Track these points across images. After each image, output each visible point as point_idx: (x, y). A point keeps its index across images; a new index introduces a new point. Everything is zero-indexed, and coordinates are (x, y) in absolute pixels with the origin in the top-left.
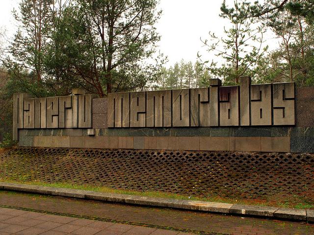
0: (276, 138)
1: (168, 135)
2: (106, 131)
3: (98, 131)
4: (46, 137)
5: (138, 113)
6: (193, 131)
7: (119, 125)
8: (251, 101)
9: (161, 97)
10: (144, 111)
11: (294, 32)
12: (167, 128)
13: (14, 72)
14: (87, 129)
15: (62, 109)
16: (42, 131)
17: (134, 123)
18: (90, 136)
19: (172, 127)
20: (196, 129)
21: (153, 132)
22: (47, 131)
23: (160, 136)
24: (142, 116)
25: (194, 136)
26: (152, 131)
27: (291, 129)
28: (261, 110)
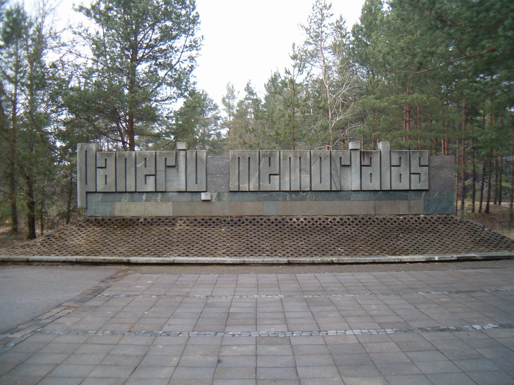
3: (215, 195)
12: (304, 192)
14: (200, 192)
16: (127, 195)
17: (266, 186)
21: (288, 197)
22: (136, 196)
23: (296, 200)
26: (287, 195)
28: (321, 183)
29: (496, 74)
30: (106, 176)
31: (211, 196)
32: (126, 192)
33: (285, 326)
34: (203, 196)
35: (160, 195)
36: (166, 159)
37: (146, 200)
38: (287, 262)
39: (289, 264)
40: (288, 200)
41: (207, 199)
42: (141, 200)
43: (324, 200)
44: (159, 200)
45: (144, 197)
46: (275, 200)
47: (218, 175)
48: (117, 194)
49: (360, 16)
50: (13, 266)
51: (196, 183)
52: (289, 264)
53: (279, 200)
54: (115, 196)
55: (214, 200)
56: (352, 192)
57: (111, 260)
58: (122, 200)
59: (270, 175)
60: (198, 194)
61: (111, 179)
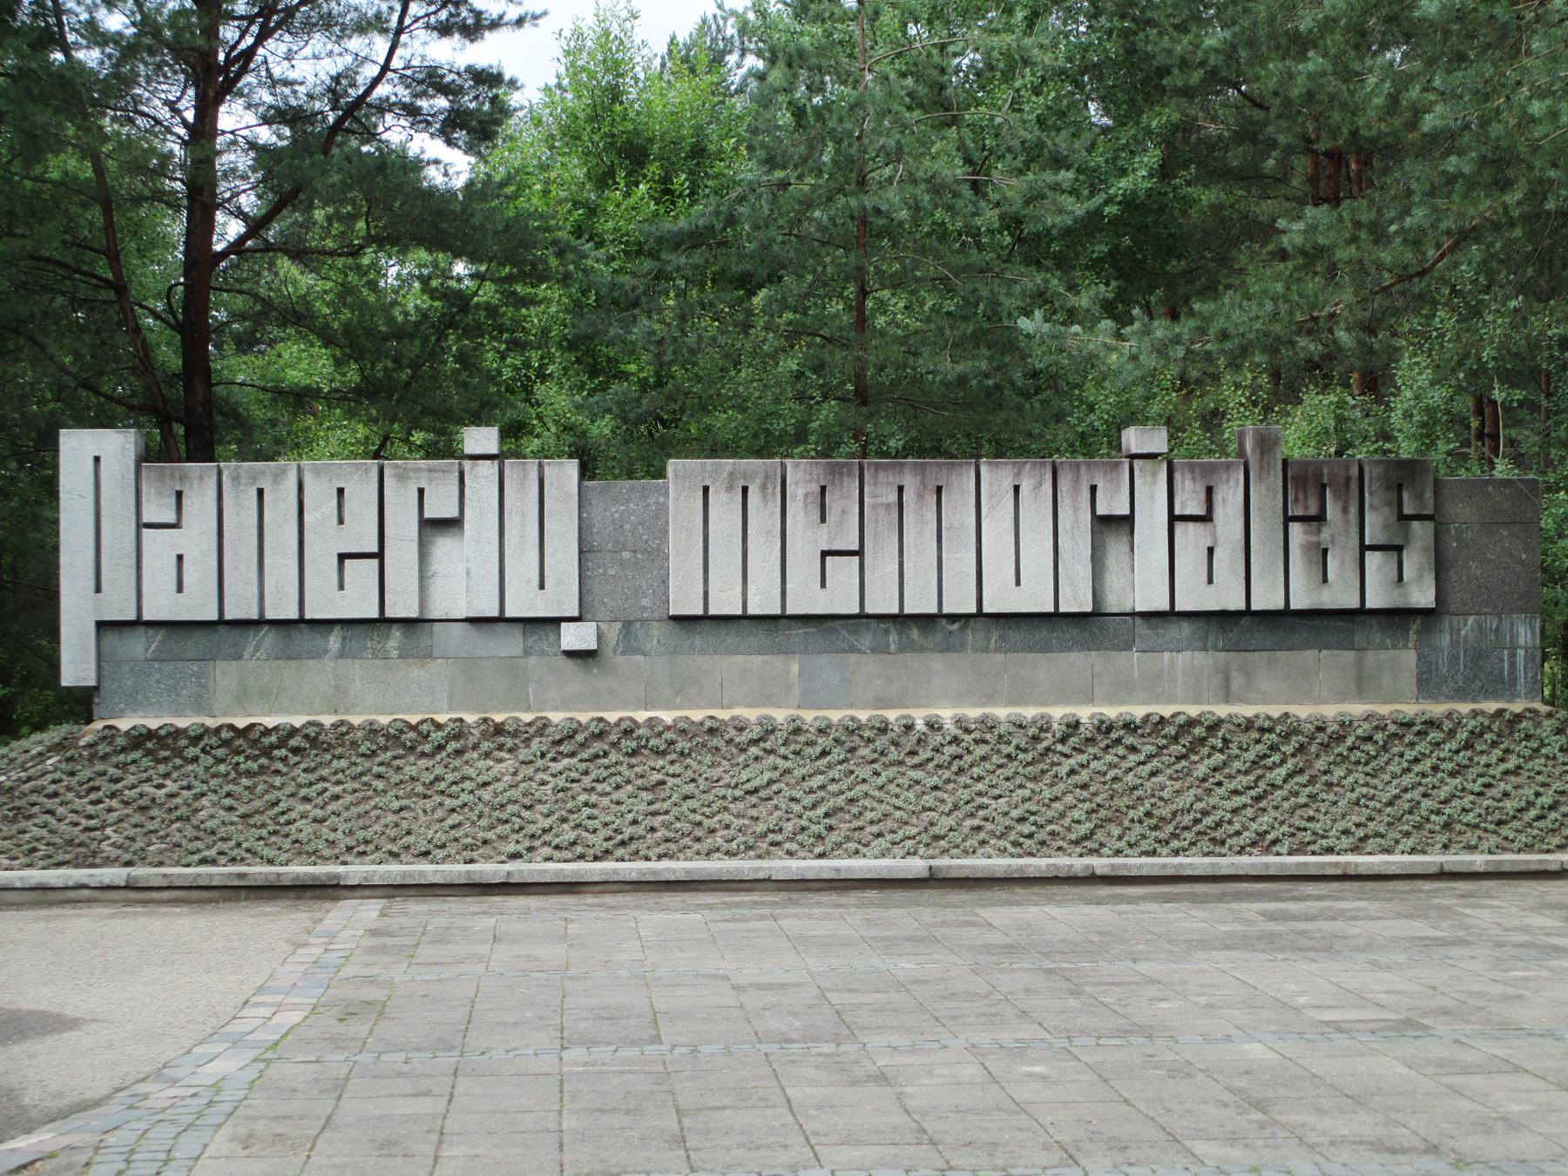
0: (1370, 655)
1: (961, 648)
2: (658, 631)
3: (613, 632)
4: (294, 664)
5: (825, 554)
6: (1071, 632)
7: (725, 602)
8: (1173, 519)
9: (932, 487)
10: (856, 547)
11: (1084, 301)
12: (954, 618)
13: (1412, 7)
14: (556, 621)
15: (402, 526)
16: (268, 638)
17: (806, 599)
18: (571, 654)
19: (980, 614)
20: (1087, 626)
22: (304, 640)
23: (921, 650)
24: (843, 571)
25: (1069, 649)
27: (1419, 621)
28: (1018, 583)
29: (187, 436)
30: (180, 558)
31: (600, 637)
32: (260, 622)
33: (911, 1104)
34: (575, 637)
35: (397, 633)
36: (421, 492)
37: (341, 655)
38: (925, 874)
39: (933, 881)
40: (893, 648)
41: (584, 647)
42: (321, 654)
43: (1031, 650)
44: (395, 653)
45: (334, 641)
46: (843, 651)
47: (626, 555)
48: (222, 629)
49: (683, 37)
50: (310, 903)
51: (542, 586)
52: (1443, 875)
53: (859, 651)
54: (216, 636)
55: (608, 652)
56: (1138, 621)
57: (314, 877)
58: (246, 655)
59: (825, 554)
60: (549, 628)
61: (200, 574)
